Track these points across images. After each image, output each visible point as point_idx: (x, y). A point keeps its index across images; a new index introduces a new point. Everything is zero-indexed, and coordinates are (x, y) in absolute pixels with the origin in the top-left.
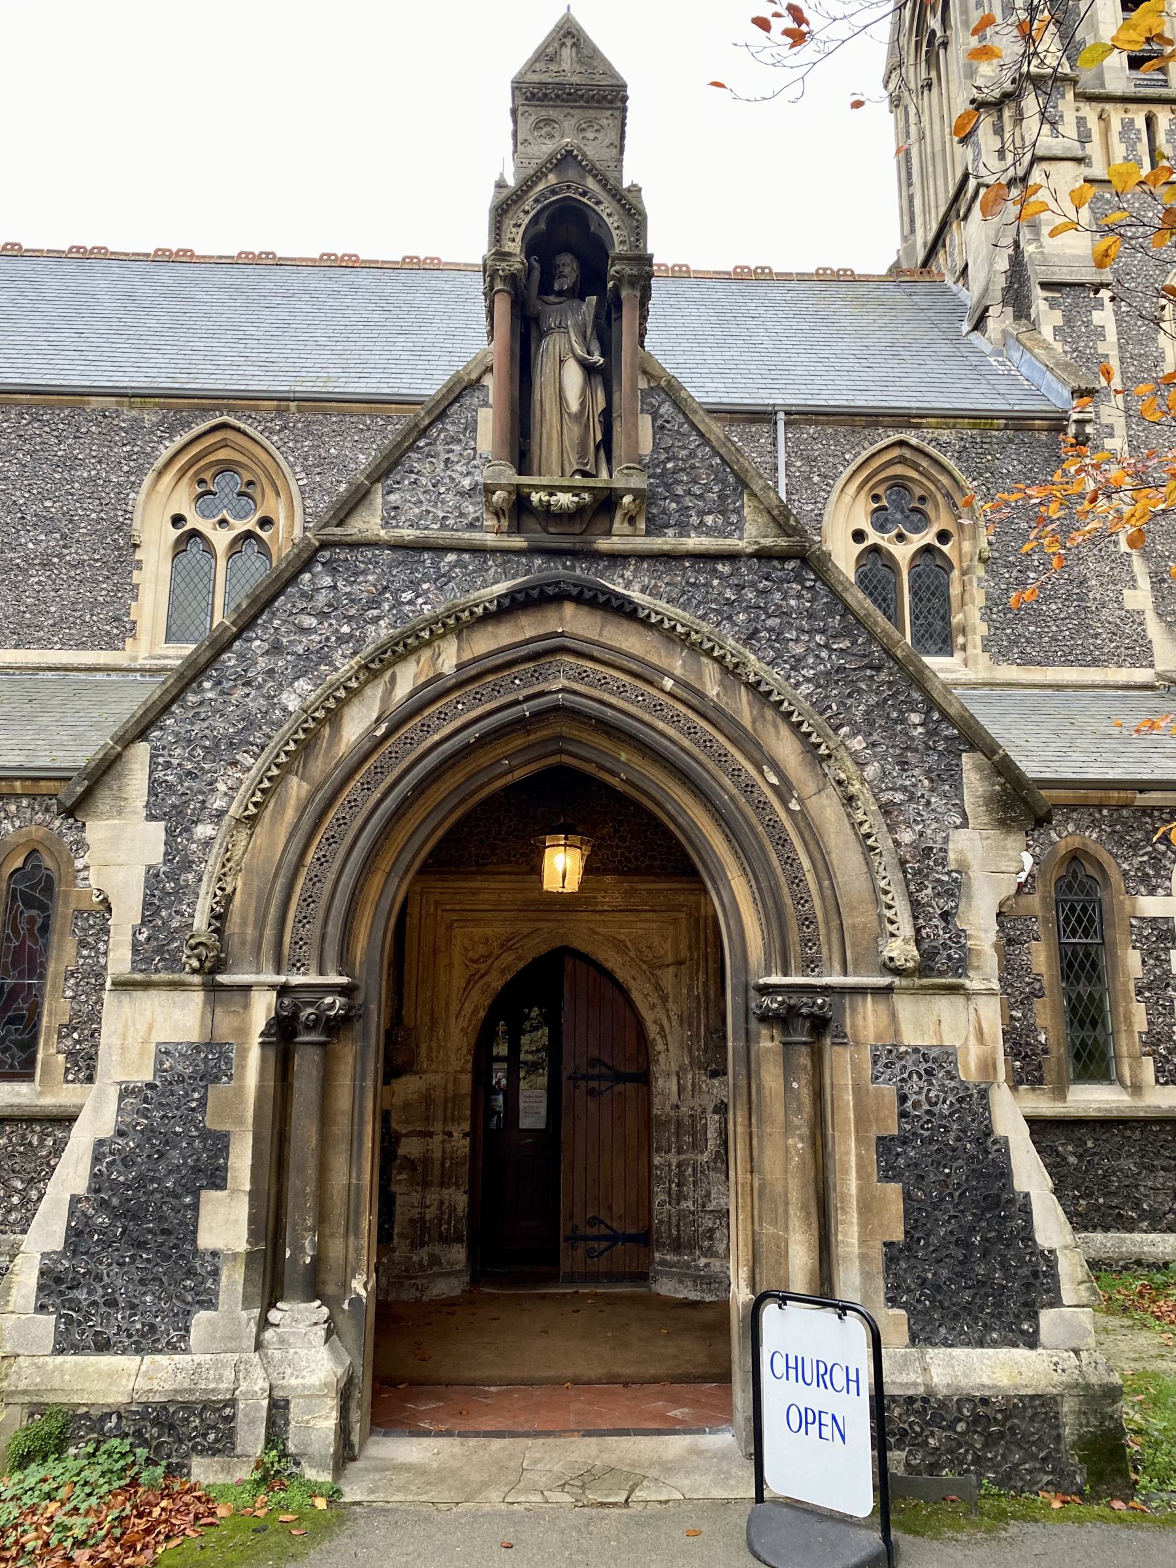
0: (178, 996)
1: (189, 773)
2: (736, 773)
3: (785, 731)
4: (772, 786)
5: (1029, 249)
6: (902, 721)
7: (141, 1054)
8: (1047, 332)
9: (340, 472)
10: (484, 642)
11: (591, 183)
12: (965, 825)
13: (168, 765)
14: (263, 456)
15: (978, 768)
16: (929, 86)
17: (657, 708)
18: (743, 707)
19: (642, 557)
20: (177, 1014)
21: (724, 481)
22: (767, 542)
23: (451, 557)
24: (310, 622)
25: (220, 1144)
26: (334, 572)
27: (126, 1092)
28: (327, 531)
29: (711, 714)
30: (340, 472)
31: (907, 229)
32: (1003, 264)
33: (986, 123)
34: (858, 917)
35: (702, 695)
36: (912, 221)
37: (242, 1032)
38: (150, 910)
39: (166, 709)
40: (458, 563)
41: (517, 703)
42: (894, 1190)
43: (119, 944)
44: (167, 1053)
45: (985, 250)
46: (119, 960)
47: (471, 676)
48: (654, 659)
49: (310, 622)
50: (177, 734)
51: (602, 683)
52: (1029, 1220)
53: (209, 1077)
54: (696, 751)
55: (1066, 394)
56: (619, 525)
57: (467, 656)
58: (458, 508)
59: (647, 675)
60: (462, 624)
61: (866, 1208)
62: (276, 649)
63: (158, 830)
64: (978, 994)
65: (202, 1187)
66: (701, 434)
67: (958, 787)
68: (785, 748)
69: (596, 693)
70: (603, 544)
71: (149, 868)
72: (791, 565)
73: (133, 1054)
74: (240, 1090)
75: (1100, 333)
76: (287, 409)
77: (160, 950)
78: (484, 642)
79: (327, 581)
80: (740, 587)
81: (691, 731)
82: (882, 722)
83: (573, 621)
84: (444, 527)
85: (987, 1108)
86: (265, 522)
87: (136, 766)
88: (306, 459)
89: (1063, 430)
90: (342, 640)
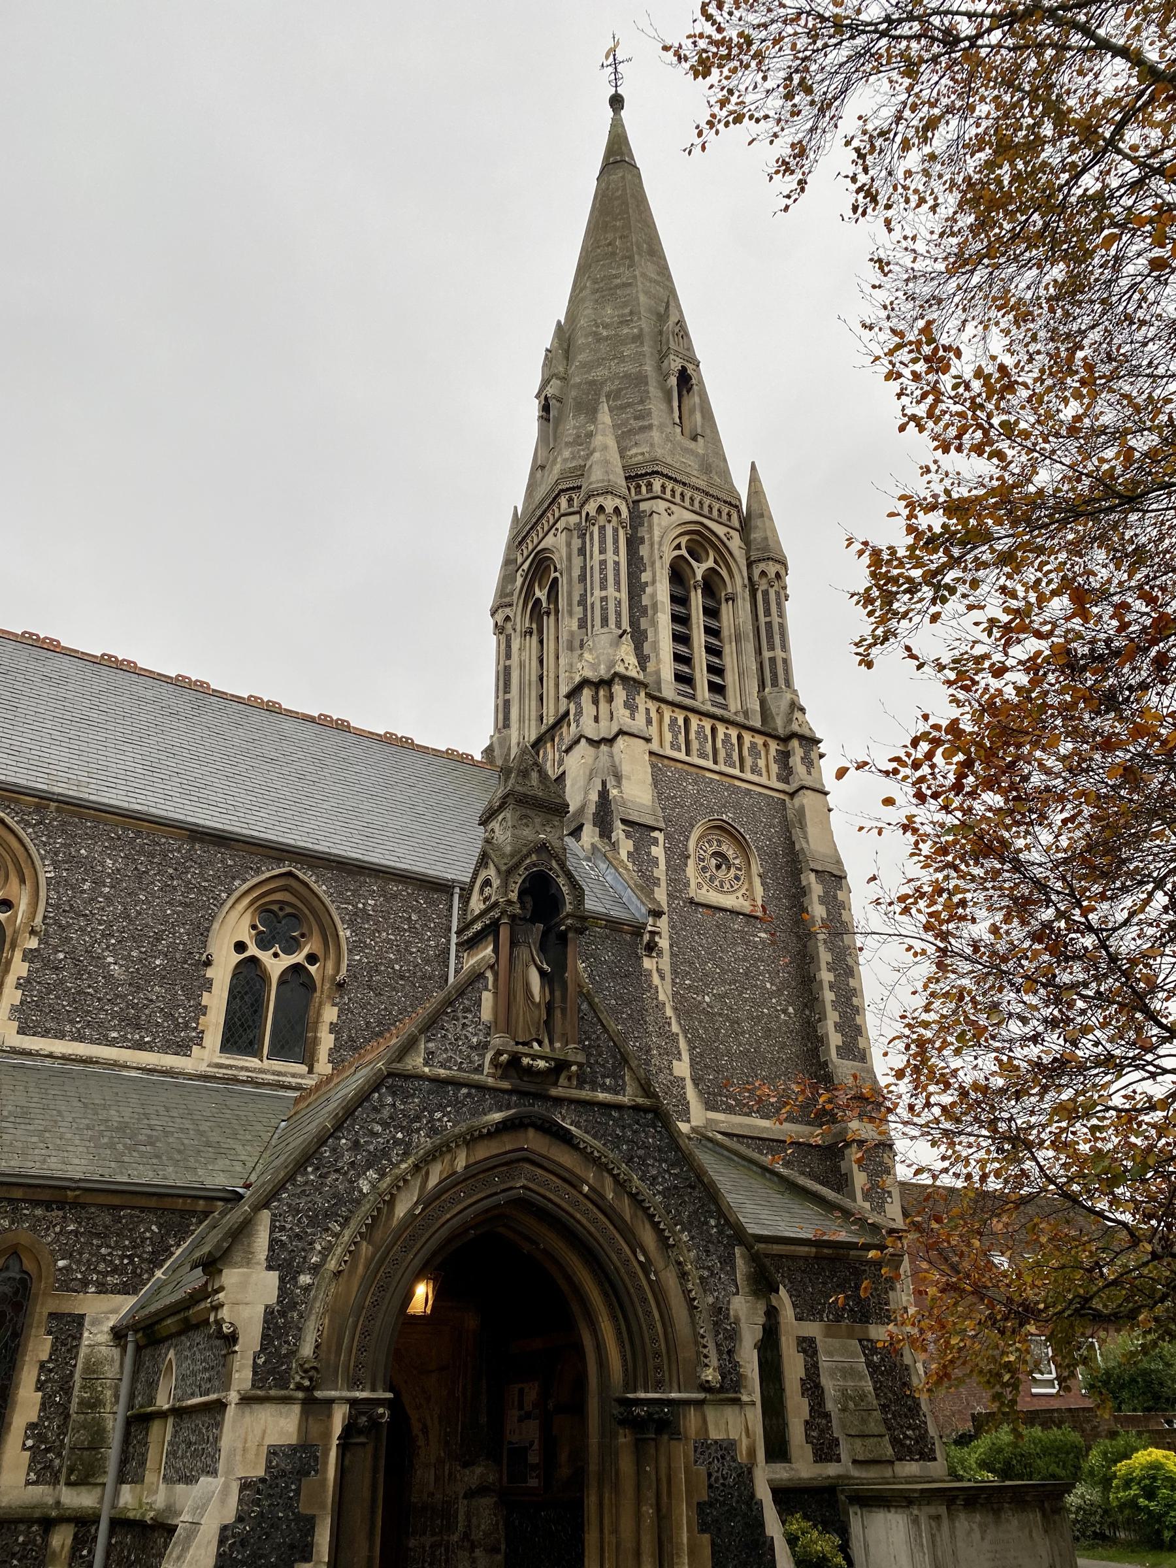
0: (284, 1408)
1: (297, 1235)
2: (619, 1252)
3: (648, 1226)
4: (640, 1262)
5: (614, 792)
6: (707, 1223)
7: (257, 1455)
8: (623, 855)
9: (86, 872)
10: (482, 1152)
11: (554, 864)
12: (737, 1293)
13: (282, 1229)
14: (15, 844)
15: (743, 1256)
16: (531, 633)
17: (576, 1204)
18: (626, 1208)
19: (571, 1101)
20: (282, 1422)
21: (614, 1057)
22: (640, 1100)
23: (464, 1091)
24: (378, 1128)
25: (308, 1525)
26: (394, 1094)
27: (245, 1485)
28: (394, 1065)
29: (609, 1211)
30: (86, 872)
31: (500, 725)
32: (594, 797)
34: (686, 1353)
35: (603, 1197)
36: (507, 717)
37: (327, 1435)
38: (266, 1338)
39: (281, 1187)
40: (469, 1095)
41: (496, 1194)
42: (706, 1538)
43: (242, 1367)
44: (275, 1453)
45: (581, 782)
46: (242, 1376)
47: (473, 1173)
48: (578, 1171)
49: (378, 1128)
50: (289, 1205)
51: (545, 1184)
52: (773, 1556)
53: (303, 1471)
54: (597, 1235)
55: (644, 910)
56: (562, 1081)
57: (472, 1160)
58: (469, 1056)
59: (573, 1182)
60: (472, 1139)
61: (692, 1553)
62: (356, 1146)
63: (273, 1277)
64: (746, 1404)
65: (296, 1561)
66: (603, 1026)
67: (733, 1268)
68: (648, 1237)
69: (541, 1191)
70: (554, 1092)
71: (267, 1307)
72: (650, 1116)
73: (251, 1456)
74: (325, 1479)
75: (655, 862)
76: (48, 807)
77: (272, 1372)
78: (482, 1152)
79: (389, 1100)
80: (624, 1127)
81: (594, 1221)
82: (695, 1224)
83: (533, 1141)
84: (460, 1069)
85: (752, 1481)
87: (261, 1228)
88: (56, 854)
89: (641, 935)
90: (397, 1142)
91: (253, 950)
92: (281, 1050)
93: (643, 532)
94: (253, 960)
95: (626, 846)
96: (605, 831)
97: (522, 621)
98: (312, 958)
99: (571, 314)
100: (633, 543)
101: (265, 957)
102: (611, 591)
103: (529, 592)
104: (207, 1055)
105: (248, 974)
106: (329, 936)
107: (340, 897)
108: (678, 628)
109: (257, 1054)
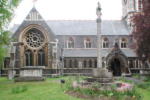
8: (132, 28)
32: (130, 23)
33: (129, 14)
68: (123, 59)
83: (117, 56)
86: (90, 42)
91: (104, 42)
92: (107, 47)
94: (104, 42)
96: (131, 27)
97: (124, 4)
98: (108, 42)
101: (105, 42)
102: (131, 2)
103: (125, 1)
104: (68, 48)
105: (122, 43)
106: (109, 40)
109: (123, 48)
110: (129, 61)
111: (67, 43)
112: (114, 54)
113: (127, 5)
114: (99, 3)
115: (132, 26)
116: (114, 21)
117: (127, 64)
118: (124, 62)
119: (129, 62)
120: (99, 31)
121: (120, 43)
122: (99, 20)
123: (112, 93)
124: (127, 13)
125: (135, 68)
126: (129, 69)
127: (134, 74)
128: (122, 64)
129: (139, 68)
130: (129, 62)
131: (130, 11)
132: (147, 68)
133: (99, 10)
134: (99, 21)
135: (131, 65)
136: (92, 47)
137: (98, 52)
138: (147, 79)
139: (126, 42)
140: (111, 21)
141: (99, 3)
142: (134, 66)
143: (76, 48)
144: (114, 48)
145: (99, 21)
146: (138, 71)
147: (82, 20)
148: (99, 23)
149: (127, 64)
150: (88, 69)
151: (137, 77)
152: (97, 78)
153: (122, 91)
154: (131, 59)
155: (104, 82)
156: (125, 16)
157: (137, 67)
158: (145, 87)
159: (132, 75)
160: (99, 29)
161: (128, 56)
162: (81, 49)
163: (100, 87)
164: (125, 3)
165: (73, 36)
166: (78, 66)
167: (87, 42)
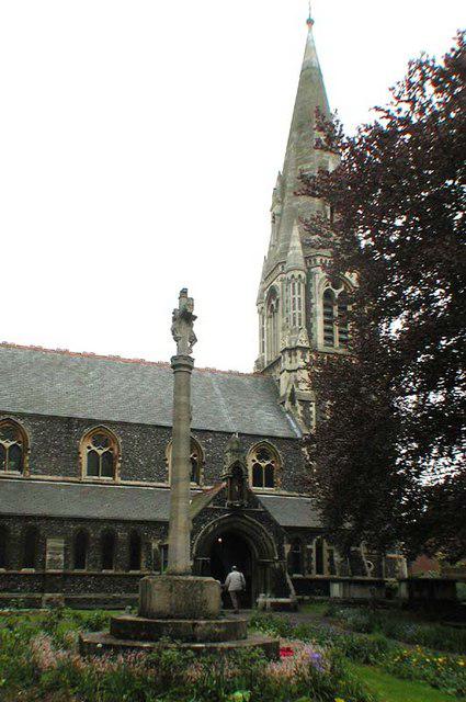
32: (289, 391)
33: (286, 355)
86: (111, 449)
93: (311, 281)
95: (300, 408)
96: (293, 403)
97: (266, 312)
99: (46, 351)
100: (308, 287)
102: (297, 311)
103: (270, 302)
105: (257, 468)
106: (276, 454)
107: (201, 438)
108: (327, 335)
110: (289, 542)
111: (250, 465)
112: (226, 511)
113: (281, 321)
114: (184, 292)
115: (297, 404)
116: (224, 373)
117: (281, 556)
118: (269, 545)
119: (287, 548)
120: (182, 407)
121: (250, 468)
122: (186, 362)
123: (247, 689)
124: (281, 348)
125: (310, 573)
126: (288, 576)
127: (307, 598)
128: (257, 555)
129: (326, 575)
130: (287, 548)
131: (290, 342)
132: (358, 574)
133: (184, 323)
134: (182, 364)
135: (297, 562)
136: (117, 472)
137: (175, 498)
138: (364, 620)
139: (273, 462)
140: (213, 371)
141: (184, 292)
142: (306, 565)
143: (36, 473)
144: (225, 484)
145: (182, 364)
146: (325, 586)
147: (72, 350)
148: (182, 376)
149: (281, 556)
150: (96, 576)
151: (324, 609)
152: (167, 618)
153: (289, 679)
154: (294, 535)
155: (199, 638)
156: (268, 358)
157: (320, 571)
158: (372, 658)
159: (301, 602)
160: (183, 399)
161: (284, 520)
162: (60, 478)
163: (188, 661)
164: (273, 311)
165: (22, 416)
166: (44, 560)
167: (93, 448)
